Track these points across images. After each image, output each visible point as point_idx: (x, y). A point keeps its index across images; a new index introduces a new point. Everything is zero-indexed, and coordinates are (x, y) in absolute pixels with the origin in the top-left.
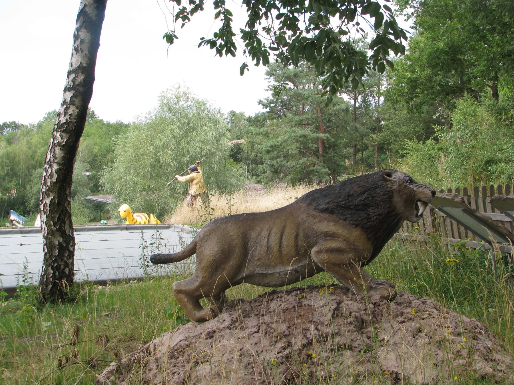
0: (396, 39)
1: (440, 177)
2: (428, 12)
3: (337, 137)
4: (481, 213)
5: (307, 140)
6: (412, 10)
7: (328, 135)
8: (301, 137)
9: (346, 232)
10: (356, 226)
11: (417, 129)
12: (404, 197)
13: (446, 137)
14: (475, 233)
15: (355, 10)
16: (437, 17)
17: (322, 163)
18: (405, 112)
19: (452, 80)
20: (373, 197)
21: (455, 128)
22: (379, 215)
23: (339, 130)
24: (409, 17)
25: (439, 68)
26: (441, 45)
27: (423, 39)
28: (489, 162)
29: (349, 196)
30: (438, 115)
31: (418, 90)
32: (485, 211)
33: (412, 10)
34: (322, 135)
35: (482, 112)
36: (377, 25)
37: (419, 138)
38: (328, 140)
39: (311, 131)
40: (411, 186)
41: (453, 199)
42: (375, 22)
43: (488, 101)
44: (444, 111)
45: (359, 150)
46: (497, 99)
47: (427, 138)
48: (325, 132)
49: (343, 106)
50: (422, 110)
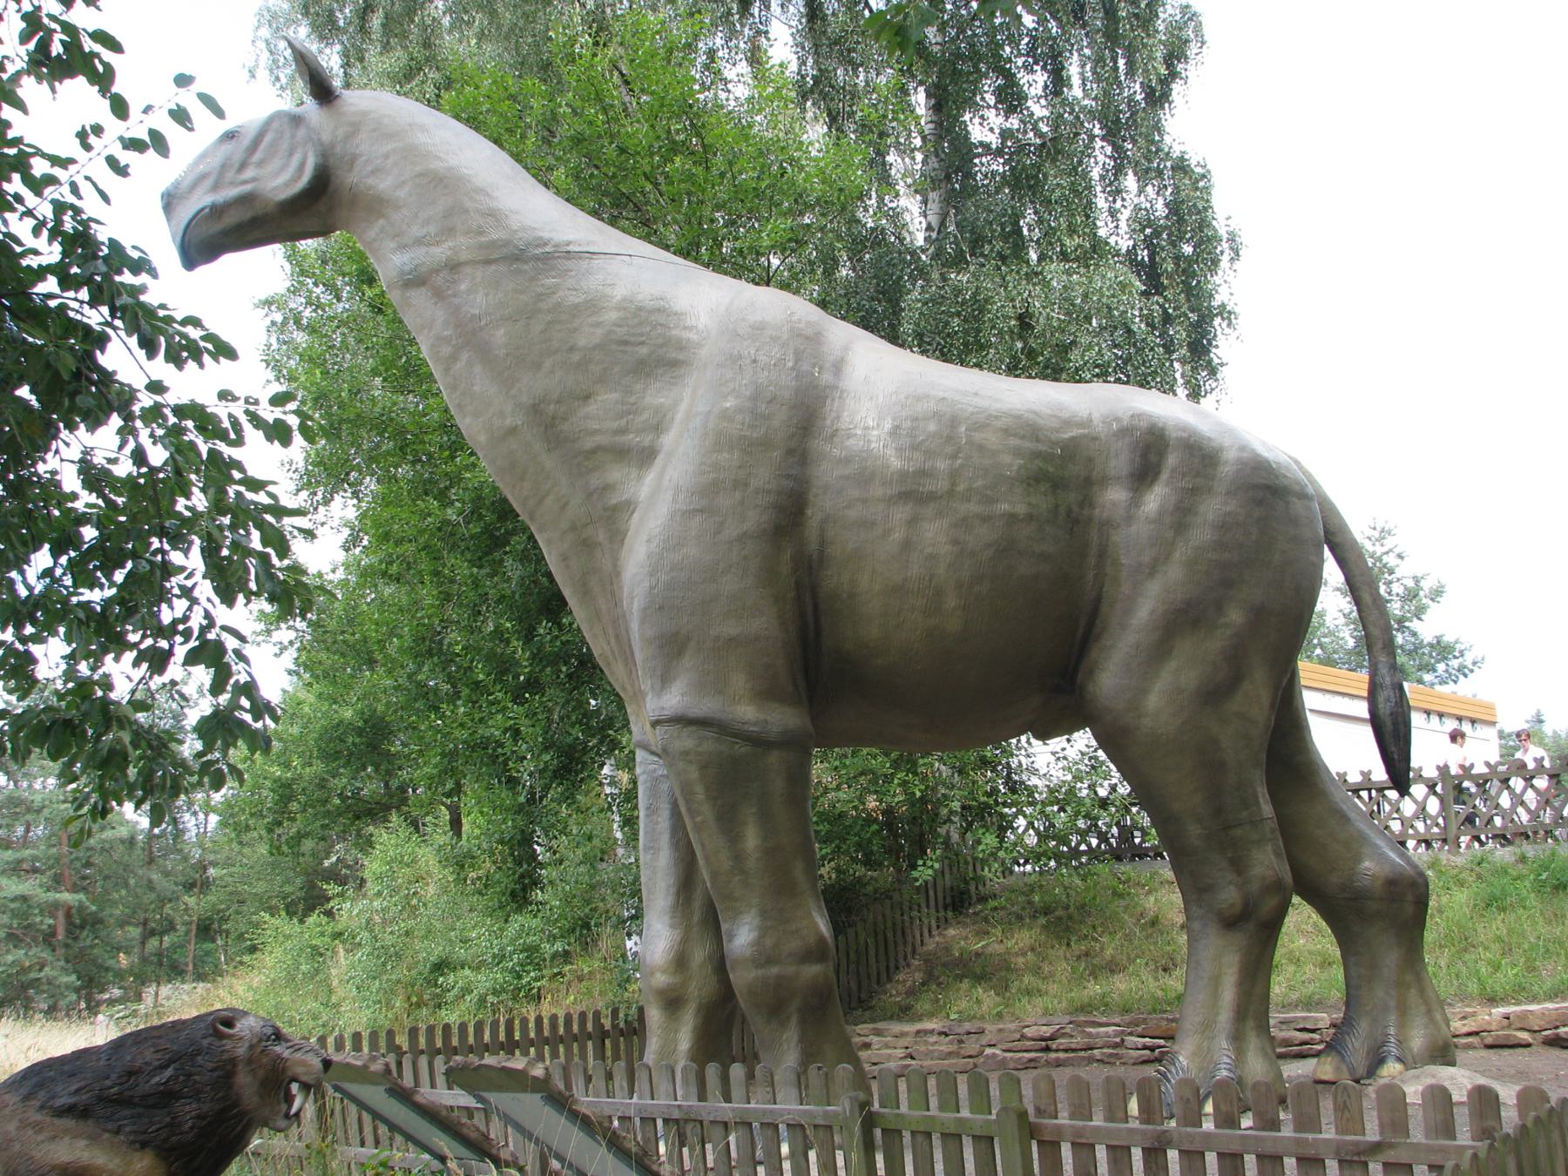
0: (256, 721)
1: (334, 999)
2: (324, 641)
3: (103, 900)
4: (426, 1094)
5: (29, 907)
6: (292, 635)
7: (81, 896)
8: (13, 900)
9: (117, 1161)
10: (144, 1145)
11: (288, 889)
12: (261, 1073)
13: (350, 911)
14: (409, 1137)
15: (170, 653)
16: (343, 655)
17: (62, 963)
18: (263, 849)
19: (371, 788)
20: (189, 1075)
21: (372, 887)
22: (198, 1117)
23: (110, 884)
24: (283, 649)
25: (342, 762)
26: (348, 714)
27: (312, 698)
28: (440, 967)
29: (130, 1074)
30: (334, 859)
31: (294, 806)
32: (433, 1086)
33: (292, 635)
34: (66, 897)
35: (427, 857)
36: (216, 689)
37: (291, 913)
38: (81, 908)
39: (41, 886)
40: (277, 1049)
41: (365, 1067)
42: (214, 680)
43: (442, 837)
44: (347, 851)
45: (153, 933)
46: (458, 834)
47: (310, 909)
48: (74, 889)
49: (123, 832)
50: (303, 849)
